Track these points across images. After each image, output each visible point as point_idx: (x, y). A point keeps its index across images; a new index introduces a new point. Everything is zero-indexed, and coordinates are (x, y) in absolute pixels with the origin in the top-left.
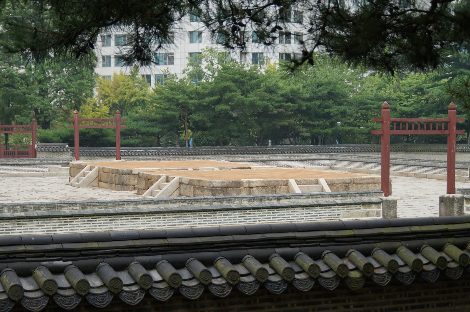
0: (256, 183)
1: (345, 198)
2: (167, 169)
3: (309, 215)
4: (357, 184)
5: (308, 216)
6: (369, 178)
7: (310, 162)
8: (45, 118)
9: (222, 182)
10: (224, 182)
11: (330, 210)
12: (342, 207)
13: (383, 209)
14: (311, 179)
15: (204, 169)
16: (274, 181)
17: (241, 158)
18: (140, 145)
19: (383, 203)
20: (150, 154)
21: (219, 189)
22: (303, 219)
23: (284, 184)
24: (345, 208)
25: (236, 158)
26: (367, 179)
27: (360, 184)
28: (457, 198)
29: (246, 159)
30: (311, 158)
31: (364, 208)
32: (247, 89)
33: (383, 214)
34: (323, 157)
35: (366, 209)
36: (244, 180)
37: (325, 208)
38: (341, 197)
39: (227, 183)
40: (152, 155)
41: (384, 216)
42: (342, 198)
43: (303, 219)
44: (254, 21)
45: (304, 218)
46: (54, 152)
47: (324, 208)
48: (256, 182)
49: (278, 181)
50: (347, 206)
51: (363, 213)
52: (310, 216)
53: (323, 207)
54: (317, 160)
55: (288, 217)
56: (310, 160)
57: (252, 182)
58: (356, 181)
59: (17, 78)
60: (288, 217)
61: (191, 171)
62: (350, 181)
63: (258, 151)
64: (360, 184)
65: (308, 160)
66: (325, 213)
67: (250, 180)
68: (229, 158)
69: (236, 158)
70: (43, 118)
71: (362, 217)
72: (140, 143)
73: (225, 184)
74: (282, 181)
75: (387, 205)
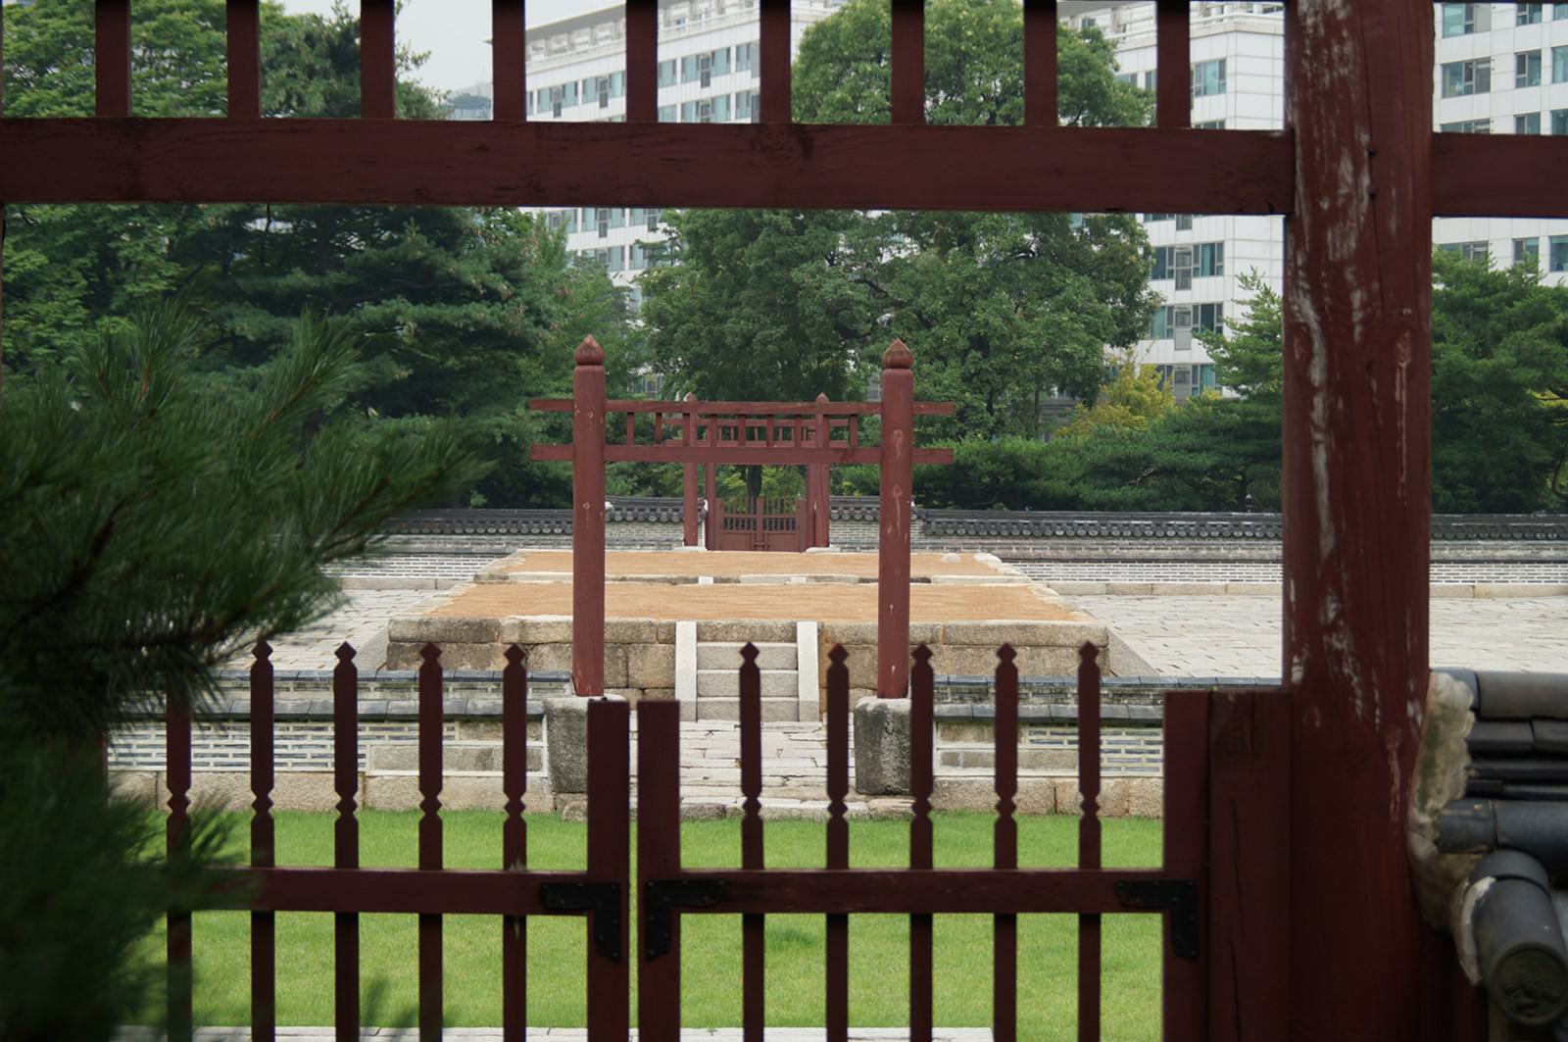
0: (548, 630)
1: (397, 694)
2: (629, 576)
3: (231, 751)
4: (959, 646)
5: (226, 756)
6: (1011, 627)
7: (1494, 569)
8: (943, 425)
9: (420, 623)
10: (427, 623)
11: (320, 737)
12: (371, 729)
13: (551, 742)
14: (769, 622)
15: (984, 581)
16: (622, 624)
17: (1239, 551)
18: (1151, 505)
19: (550, 720)
20: (1171, 533)
21: (408, 645)
22: (208, 764)
23: (662, 637)
24: (386, 734)
25: (1223, 551)
26: (1000, 628)
27: (971, 645)
28: (895, 714)
29: (1256, 554)
30: (1499, 554)
31: (470, 737)
32: (1493, 330)
33: (551, 762)
34: (1545, 554)
35: (479, 738)
36: (509, 619)
37: (301, 729)
38: (381, 689)
39: (439, 625)
40: (1177, 535)
41: (555, 769)
42: (388, 695)
43: (208, 764)
44: (894, 98)
45: (212, 760)
46: (653, 523)
47: (297, 729)
48: (548, 625)
49: (634, 626)
50: (393, 725)
51: (465, 753)
52: (235, 756)
53: (291, 726)
54: (1523, 562)
55: (145, 755)
56: (1496, 562)
57: (535, 625)
58: (954, 637)
59: (861, 308)
60: (145, 755)
61: (706, 588)
62: (929, 635)
63: (1544, 530)
64: (971, 645)
65: (1489, 562)
66: (300, 746)
67: (529, 618)
68: (1196, 550)
69: (1223, 551)
70: (939, 425)
71: (460, 769)
72: (1149, 499)
73: (432, 629)
74: (651, 624)
75: (569, 729)
